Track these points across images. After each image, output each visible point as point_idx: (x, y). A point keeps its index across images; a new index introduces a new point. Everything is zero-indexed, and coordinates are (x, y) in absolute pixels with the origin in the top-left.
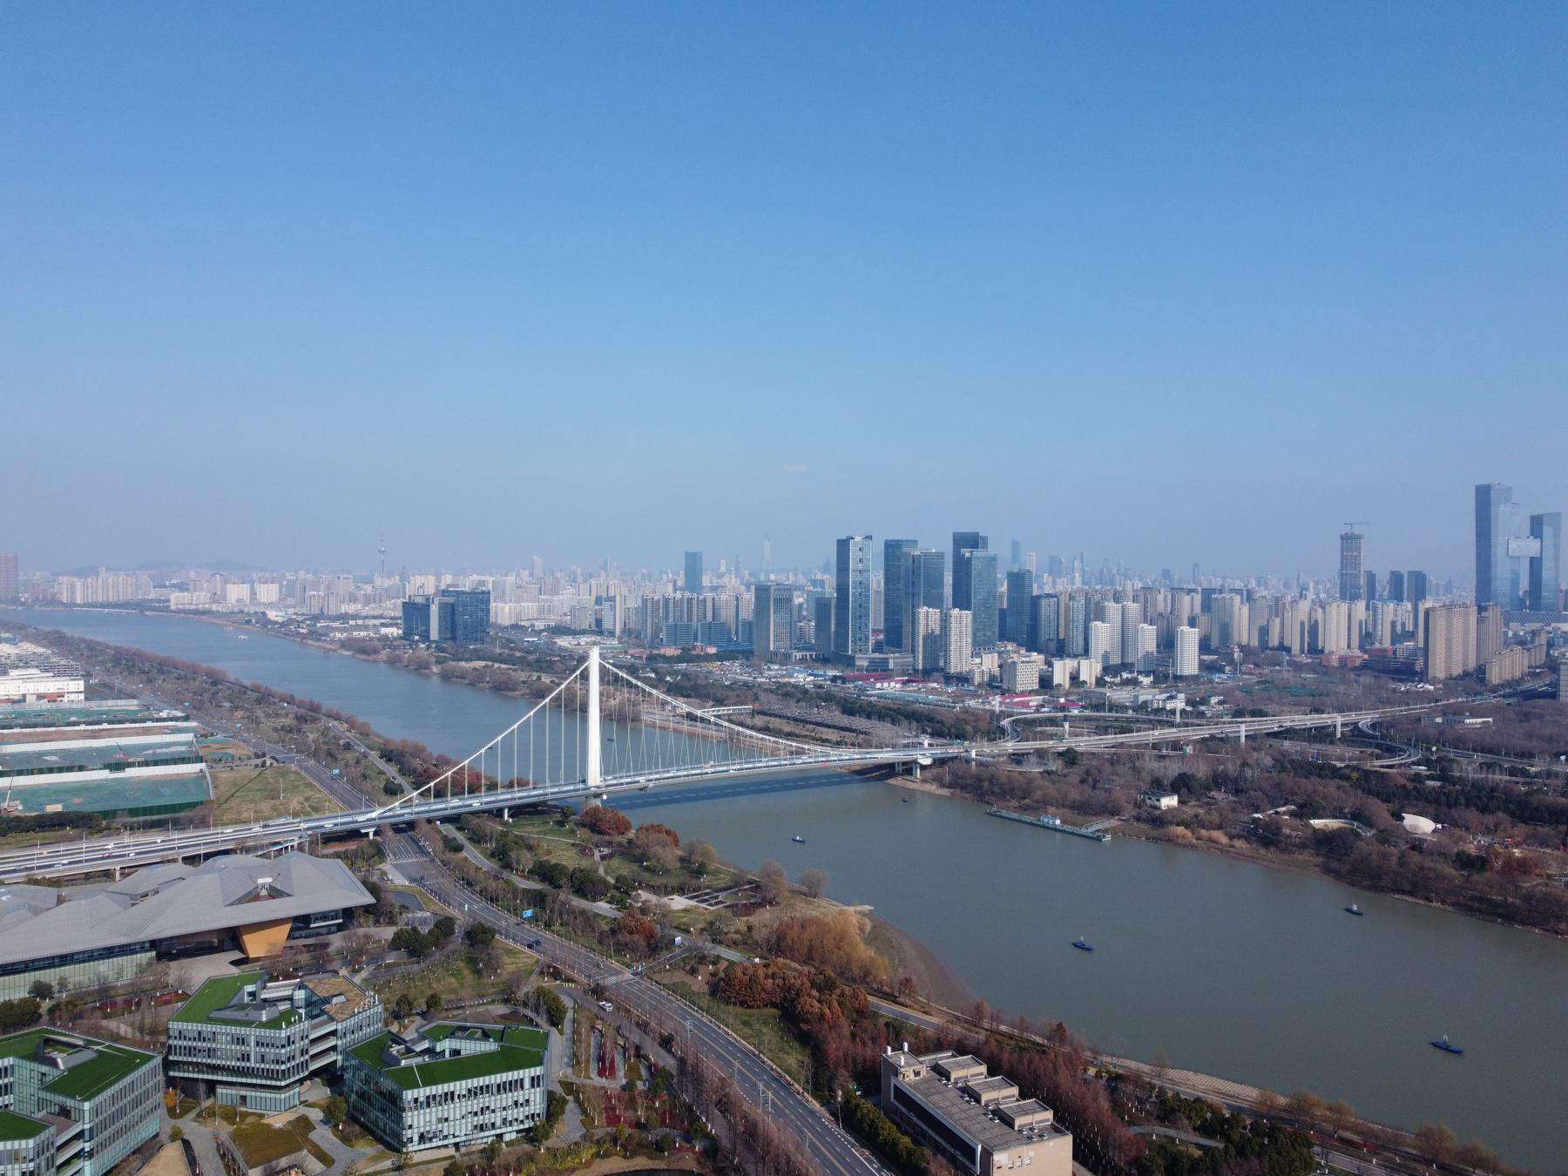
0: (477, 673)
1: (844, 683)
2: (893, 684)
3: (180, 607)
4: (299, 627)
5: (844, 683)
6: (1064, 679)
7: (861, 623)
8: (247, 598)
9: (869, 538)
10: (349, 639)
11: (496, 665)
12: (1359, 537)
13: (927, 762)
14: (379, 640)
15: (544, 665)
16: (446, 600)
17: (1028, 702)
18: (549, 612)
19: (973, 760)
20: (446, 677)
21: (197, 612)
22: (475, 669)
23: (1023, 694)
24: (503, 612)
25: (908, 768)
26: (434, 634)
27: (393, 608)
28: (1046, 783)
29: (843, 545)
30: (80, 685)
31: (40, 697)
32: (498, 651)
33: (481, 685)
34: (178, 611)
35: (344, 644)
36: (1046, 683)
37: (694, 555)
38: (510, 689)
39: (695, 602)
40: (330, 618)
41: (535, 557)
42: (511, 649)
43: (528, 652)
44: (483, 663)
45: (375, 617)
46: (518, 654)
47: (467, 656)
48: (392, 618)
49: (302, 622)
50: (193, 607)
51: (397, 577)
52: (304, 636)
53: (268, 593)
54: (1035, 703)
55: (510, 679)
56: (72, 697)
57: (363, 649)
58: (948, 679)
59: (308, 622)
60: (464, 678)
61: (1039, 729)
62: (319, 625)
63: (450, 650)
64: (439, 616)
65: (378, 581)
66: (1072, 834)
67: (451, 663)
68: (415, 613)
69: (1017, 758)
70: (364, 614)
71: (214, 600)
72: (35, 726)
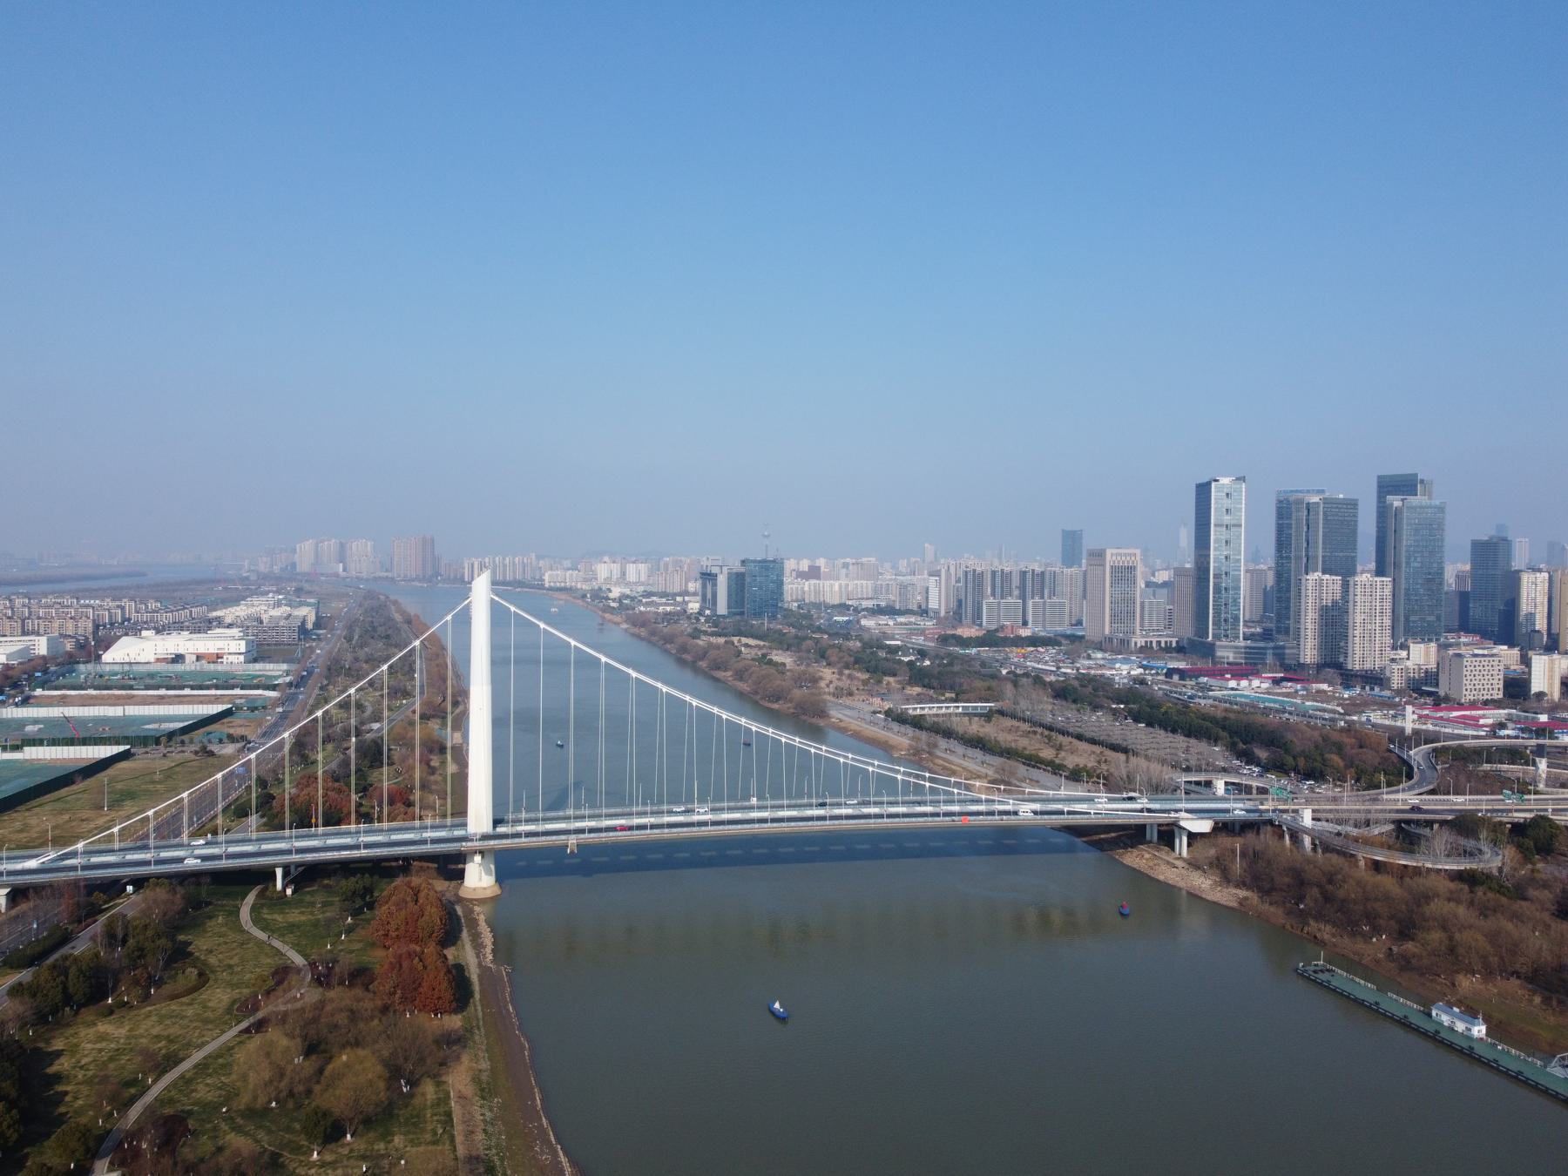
2: (1256, 683)
6: (1551, 685)
13: (1204, 826)
17: (1476, 719)
19: (1306, 831)
23: (1473, 705)
24: (795, 590)
25: (1167, 835)
28: (1461, 910)
29: (1203, 491)
30: (242, 646)
31: (199, 657)
34: (551, 589)
36: (1516, 689)
37: (1074, 533)
39: (1029, 576)
54: (1490, 721)
56: (232, 658)
58: (1348, 678)
61: (1487, 767)
66: (1517, 1078)
69: (1407, 833)
72: (208, 688)
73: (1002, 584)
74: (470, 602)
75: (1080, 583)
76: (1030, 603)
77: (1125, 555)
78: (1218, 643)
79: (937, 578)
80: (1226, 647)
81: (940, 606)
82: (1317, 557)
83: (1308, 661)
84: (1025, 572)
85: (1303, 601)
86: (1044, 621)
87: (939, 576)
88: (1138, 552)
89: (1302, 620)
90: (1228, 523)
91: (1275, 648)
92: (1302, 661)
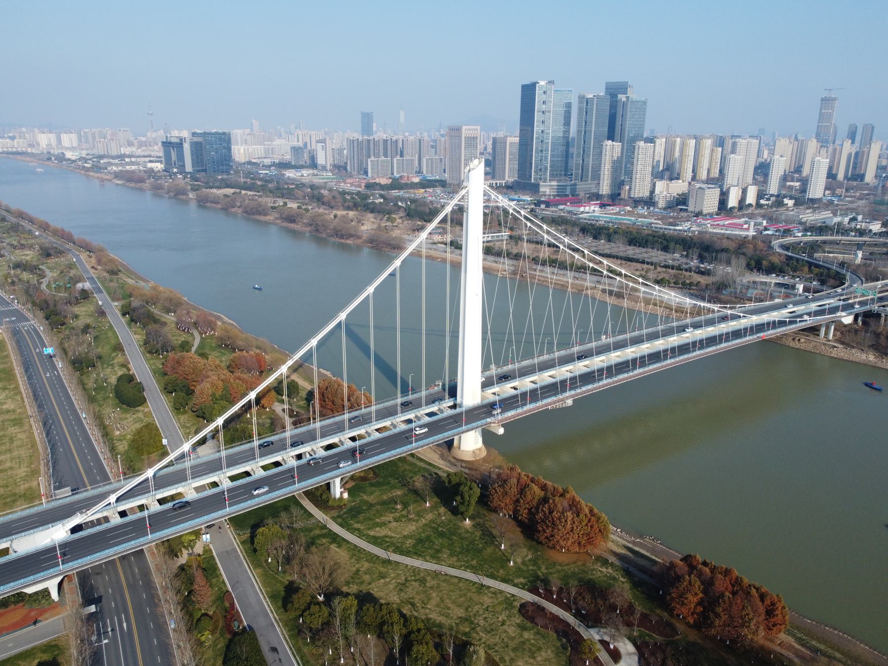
0: (229, 199)
3: (5, 150)
4: (86, 163)
5: (547, 206)
8: (54, 143)
9: (551, 82)
10: (121, 171)
11: (243, 192)
12: (834, 99)
14: (145, 172)
15: (285, 192)
16: (196, 139)
18: (273, 153)
20: (203, 203)
21: (17, 153)
22: (225, 196)
24: (240, 152)
26: (189, 168)
27: (158, 150)
29: (528, 92)
32: (242, 180)
33: (233, 210)
35: (117, 175)
37: (368, 114)
38: (260, 214)
39: (389, 142)
40: (113, 158)
41: (253, 121)
42: (252, 179)
43: (266, 181)
44: (232, 191)
45: (145, 157)
46: (259, 183)
47: (217, 184)
48: (158, 157)
49: (90, 159)
50: (14, 150)
51: (162, 131)
52: (88, 170)
53: (69, 140)
55: (260, 205)
57: (133, 180)
59: (95, 160)
60: (218, 203)
62: (102, 161)
63: (202, 180)
64: (192, 152)
65: (149, 134)
67: (204, 190)
68: (172, 147)
70: (137, 154)
71: (31, 145)
74: (467, 192)
75: (418, 144)
76: (395, 160)
77: (472, 130)
78: (541, 183)
80: (545, 186)
81: (326, 162)
82: (591, 131)
84: (387, 140)
85: (603, 158)
87: (325, 143)
88: (479, 128)
89: (602, 170)
90: (544, 110)
91: (572, 185)
92: (601, 193)
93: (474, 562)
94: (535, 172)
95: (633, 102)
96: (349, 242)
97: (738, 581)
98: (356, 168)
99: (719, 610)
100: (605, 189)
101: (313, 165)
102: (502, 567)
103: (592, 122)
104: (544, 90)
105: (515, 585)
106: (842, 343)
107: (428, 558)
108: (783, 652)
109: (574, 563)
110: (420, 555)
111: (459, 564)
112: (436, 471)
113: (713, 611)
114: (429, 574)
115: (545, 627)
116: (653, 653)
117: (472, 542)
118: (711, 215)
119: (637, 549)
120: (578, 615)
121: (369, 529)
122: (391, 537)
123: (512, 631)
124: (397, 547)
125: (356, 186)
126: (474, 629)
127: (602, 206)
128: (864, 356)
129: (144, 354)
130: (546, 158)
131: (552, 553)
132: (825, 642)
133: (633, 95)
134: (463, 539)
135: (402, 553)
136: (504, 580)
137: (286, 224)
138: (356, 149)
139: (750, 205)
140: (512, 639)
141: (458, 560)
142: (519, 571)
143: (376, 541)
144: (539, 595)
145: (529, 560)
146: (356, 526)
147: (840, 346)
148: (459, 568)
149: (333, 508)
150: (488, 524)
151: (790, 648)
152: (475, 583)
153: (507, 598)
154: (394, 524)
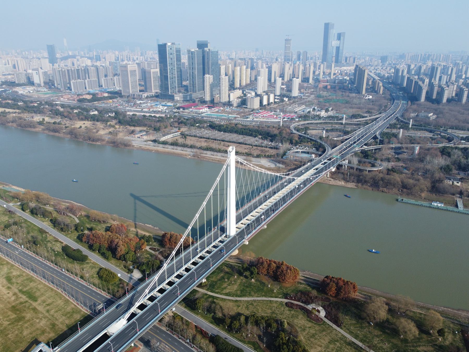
1: (184, 109)
5: (184, 109)
7: (173, 81)
12: (290, 40)
37: (51, 46)
39: (80, 71)
73: (72, 74)
77: (133, 66)
79: (37, 71)
80: (177, 96)
81: (40, 82)
83: (208, 100)
86: (92, 87)
87: (38, 70)
92: (206, 100)
93: (263, 294)
94: (170, 89)
95: (212, 52)
96: (98, 143)
97: (344, 281)
98: (63, 86)
99: (342, 290)
100: (208, 98)
101: (30, 83)
102: (273, 293)
103: (195, 63)
104: (170, 47)
105: (280, 298)
106: (333, 178)
107: (248, 296)
108: (358, 298)
109: (292, 286)
110: (245, 296)
111: (259, 295)
112: (228, 263)
113: (340, 291)
114: (252, 302)
115: (297, 308)
116: (328, 308)
117: (258, 287)
118: (257, 109)
119: (305, 276)
120: (302, 302)
121: (222, 291)
122: (232, 292)
123: (288, 312)
124: (236, 295)
125: (72, 100)
126: (277, 315)
127: (209, 107)
128: (340, 183)
129: (60, 233)
130: (175, 81)
131: (284, 284)
132: (365, 292)
133: (211, 47)
134: (255, 286)
135: (239, 297)
136: (276, 297)
137: (52, 133)
138: (61, 76)
139: (272, 103)
140: (289, 314)
141: (258, 294)
142: (279, 293)
143: (227, 294)
144: (288, 299)
145: (279, 288)
146: (217, 291)
147: (332, 180)
148: (260, 297)
149: (204, 286)
150: (259, 279)
151: (359, 296)
152: (268, 301)
153: (280, 303)
154: (229, 287)
